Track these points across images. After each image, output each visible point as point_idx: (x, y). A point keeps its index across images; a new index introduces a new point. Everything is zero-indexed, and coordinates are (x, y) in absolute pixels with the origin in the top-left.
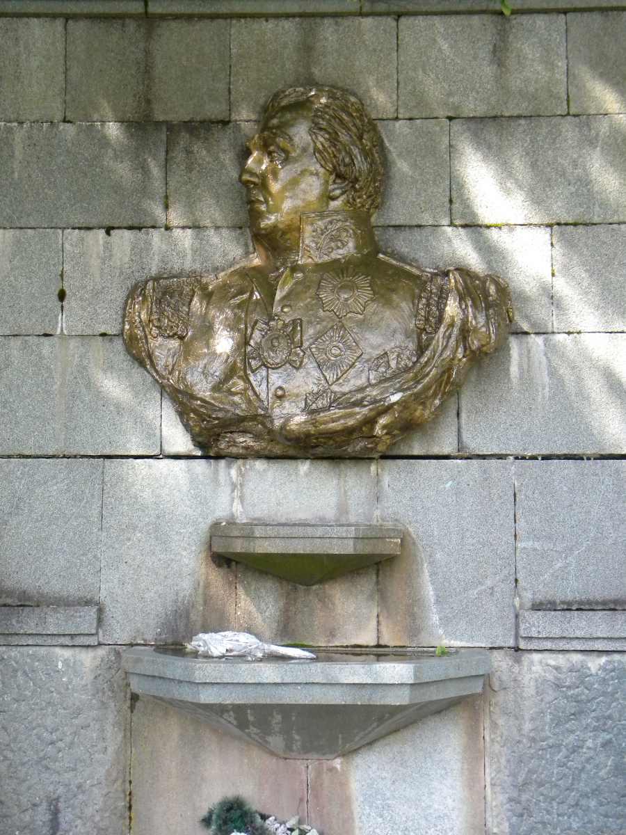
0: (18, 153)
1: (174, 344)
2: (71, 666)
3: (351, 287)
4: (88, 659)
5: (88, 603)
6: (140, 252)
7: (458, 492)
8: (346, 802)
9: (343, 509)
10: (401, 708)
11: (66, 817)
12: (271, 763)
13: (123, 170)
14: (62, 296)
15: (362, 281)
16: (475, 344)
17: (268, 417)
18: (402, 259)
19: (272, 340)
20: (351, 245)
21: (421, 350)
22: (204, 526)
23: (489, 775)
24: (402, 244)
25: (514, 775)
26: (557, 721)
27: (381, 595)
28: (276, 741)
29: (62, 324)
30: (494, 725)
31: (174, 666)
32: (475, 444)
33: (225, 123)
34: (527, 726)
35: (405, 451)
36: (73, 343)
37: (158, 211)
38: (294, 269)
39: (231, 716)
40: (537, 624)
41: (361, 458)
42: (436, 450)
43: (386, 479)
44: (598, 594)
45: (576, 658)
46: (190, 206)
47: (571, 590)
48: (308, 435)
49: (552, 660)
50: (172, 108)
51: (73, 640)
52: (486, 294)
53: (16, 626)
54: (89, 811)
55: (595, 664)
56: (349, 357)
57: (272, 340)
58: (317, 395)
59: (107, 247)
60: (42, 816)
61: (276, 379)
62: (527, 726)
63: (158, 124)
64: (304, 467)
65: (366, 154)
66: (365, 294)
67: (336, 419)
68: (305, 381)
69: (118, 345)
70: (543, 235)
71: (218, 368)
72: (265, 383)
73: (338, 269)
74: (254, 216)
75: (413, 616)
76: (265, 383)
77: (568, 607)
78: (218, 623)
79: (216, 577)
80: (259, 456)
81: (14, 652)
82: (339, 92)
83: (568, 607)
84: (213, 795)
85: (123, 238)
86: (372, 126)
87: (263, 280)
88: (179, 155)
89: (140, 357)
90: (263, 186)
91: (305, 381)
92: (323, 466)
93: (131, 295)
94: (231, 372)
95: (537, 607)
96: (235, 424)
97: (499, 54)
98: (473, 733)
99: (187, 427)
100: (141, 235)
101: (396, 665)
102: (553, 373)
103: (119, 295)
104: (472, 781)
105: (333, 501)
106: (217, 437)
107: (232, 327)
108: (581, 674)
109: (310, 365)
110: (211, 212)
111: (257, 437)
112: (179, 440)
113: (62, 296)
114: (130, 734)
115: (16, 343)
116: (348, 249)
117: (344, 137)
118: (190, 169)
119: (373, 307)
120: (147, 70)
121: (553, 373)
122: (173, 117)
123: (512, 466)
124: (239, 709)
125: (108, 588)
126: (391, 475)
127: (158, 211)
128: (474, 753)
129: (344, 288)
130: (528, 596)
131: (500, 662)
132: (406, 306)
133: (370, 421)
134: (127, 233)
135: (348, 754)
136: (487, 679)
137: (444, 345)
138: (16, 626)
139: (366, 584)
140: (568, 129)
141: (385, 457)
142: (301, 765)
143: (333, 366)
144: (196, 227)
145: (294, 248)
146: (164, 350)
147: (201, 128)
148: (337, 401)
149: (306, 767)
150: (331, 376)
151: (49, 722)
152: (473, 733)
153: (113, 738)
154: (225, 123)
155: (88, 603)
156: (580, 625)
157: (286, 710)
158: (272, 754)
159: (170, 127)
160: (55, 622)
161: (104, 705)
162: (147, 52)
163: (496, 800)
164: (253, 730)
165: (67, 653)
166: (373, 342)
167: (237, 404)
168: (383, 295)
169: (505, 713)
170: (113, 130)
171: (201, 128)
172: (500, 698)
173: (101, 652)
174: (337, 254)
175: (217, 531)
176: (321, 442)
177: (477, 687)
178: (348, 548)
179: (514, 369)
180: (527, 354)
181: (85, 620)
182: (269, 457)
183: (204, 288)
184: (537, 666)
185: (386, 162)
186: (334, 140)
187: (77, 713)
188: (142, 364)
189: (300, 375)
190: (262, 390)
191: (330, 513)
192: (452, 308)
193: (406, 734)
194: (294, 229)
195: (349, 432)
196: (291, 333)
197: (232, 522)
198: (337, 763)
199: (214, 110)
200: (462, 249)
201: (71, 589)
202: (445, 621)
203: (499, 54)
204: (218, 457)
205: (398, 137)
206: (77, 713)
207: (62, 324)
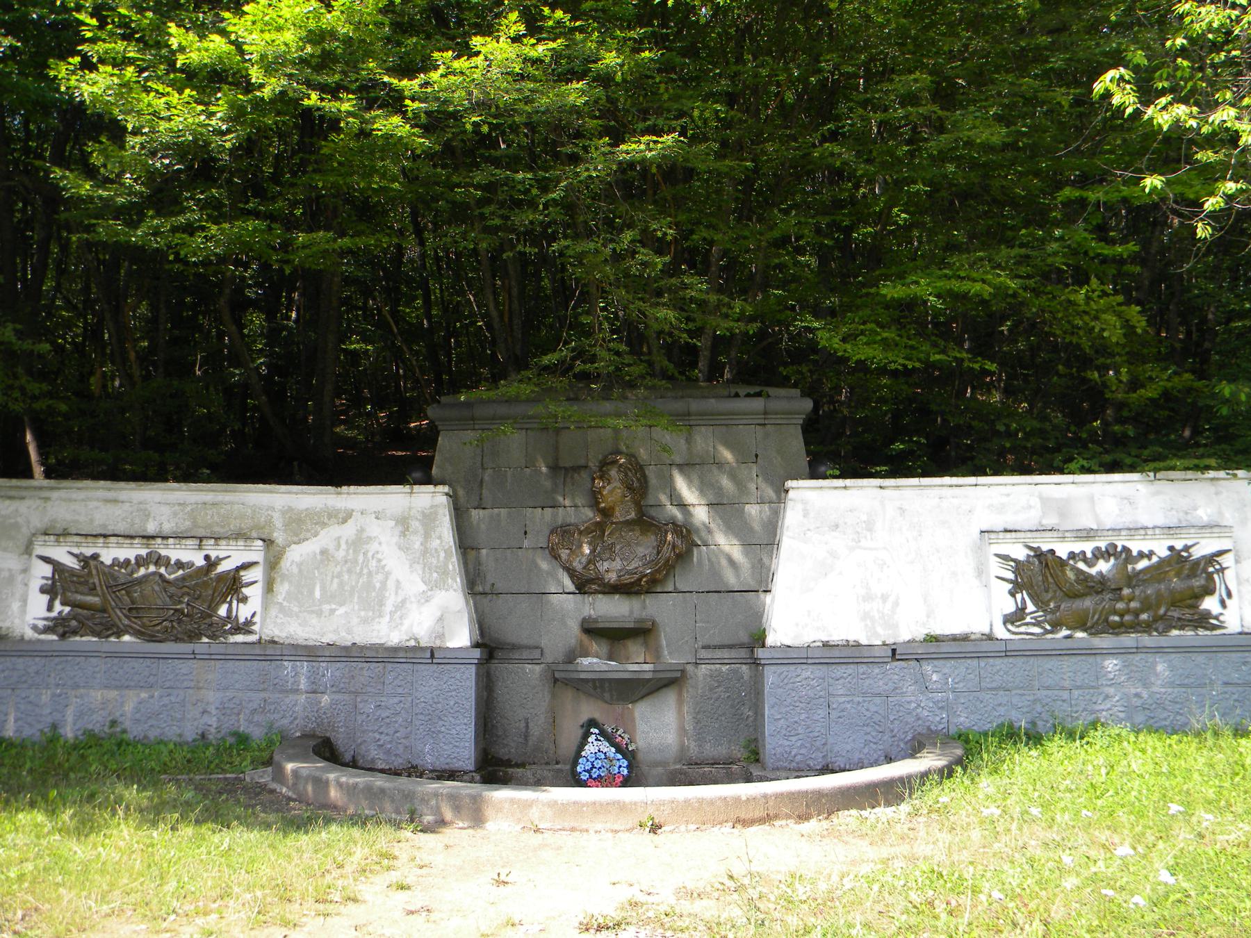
0: (509, 480)
1: (568, 551)
2: (532, 671)
3: (633, 530)
4: (537, 668)
5: (537, 648)
6: (554, 516)
7: (674, 605)
8: (633, 720)
9: (631, 612)
10: (648, 680)
11: (531, 725)
12: (606, 706)
13: (548, 484)
14: (526, 533)
15: (637, 528)
16: (677, 551)
17: (603, 579)
18: (653, 518)
19: (604, 549)
20: (633, 514)
21: (658, 553)
22: (580, 619)
23: (686, 709)
24: (653, 512)
25: (695, 709)
26: (711, 690)
27: (646, 644)
28: (607, 695)
29: (526, 544)
30: (688, 691)
31: (571, 667)
32: (681, 587)
33: (586, 467)
34: (700, 691)
35: (654, 590)
36: (530, 551)
37: (560, 499)
38: (612, 523)
39: (590, 684)
40: (704, 654)
41: (638, 593)
42: (666, 590)
43: (647, 602)
44: (726, 642)
45: (718, 666)
46: (573, 499)
47: (717, 641)
48: (617, 585)
49: (709, 667)
50: (566, 462)
51: (533, 662)
52: (682, 532)
53: (511, 656)
54: (540, 722)
55: (725, 668)
56: (632, 556)
57: (604, 549)
58: (621, 570)
59: (542, 515)
60: (523, 725)
61: (606, 565)
62: (700, 691)
63: (561, 468)
64: (617, 597)
65: (638, 480)
66: (637, 533)
67: (627, 579)
68: (617, 564)
69: (547, 551)
70: (706, 508)
71: (584, 560)
72: (603, 566)
73: (628, 523)
74: (598, 503)
75: (658, 652)
76: (603, 566)
77: (715, 647)
78: (586, 655)
79: (585, 638)
80: (600, 593)
81: (511, 666)
82: (632, 456)
83: (715, 647)
84: (584, 718)
85: (548, 511)
86: (641, 467)
87: (600, 526)
88: (568, 480)
89: (556, 557)
90: (600, 493)
91: (617, 564)
92: (624, 596)
93: (552, 532)
94: (589, 562)
95: (704, 647)
96: (591, 581)
97: (689, 441)
98: (680, 694)
99: (573, 582)
100: (555, 510)
101: (448, 517)
102: (709, 560)
103: (547, 532)
104: (680, 711)
105: (628, 609)
106: (584, 586)
107: (590, 543)
108: (720, 671)
109: (618, 559)
110: (580, 501)
111: (599, 586)
112: (570, 586)
113: (526, 533)
114: (554, 696)
115: (509, 551)
116: (633, 515)
117: (630, 474)
118: (573, 484)
119: (640, 538)
120: (556, 448)
121: (709, 560)
122: (567, 465)
123: (695, 596)
124: (594, 680)
125: (544, 642)
126: (649, 600)
127: (560, 499)
128: (680, 701)
129: (630, 531)
130: (700, 643)
131: (690, 668)
132: (653, 537)
133: (640, 580)
134: (550, 509)
135: (634, 702)
136: (683, 671)
137: (667, 552)
138: (511, 656)
139: (640, 640)
140: (714, 468)
141: (647, 592)
142: (616, 707)
143: (626, 560)
144: (576, 506)
145: (612, 515)
146: (564, 554)
147: (577, 469)
148: (630, 573)
149: (618, 708)
150: (625, 563)
151: (524, 691)
152: (680, 694)
153: (547, 697)
154: (586, 467)
155: (537, 648)
156: (719, 654)
157: (610, 681)
158: (606, 702)
159: (566, 469)
160: (526, 654)
161: (544, 685)
162: (557, 442)
163: (688, 718)
164: (598, 690)
165: (530, 666)
166: (641, 551)
167: (592, 574)
168: (644, 532)
169: (692, 687)
170: (544, 469)
171: (577, 469)
172: (690, 681)
173: (542, 666)
174: (628, 518)
175: (584, 621)
176: (1121, 221)
177: (678, 675)
178: (632, 625)
179: (695, 559)
180: (700, 553)
181: (537, 654)
182: (604, 593)
183: (579, 530)
184: (703, 669)
185: (646, 482)
186: (626, 475)
187: (534, 687)
188: (556, 559)
189: (614, 563)
190: (600, 569)
191: (627, 614)
192: (669, 537)
193: (655, 695)
194: (612, 508)
195: (632, 584)
196: (611, 548)
197: (590, 617)
198: (630, 706)
199: (582, 462)
200: (677, 513)
201: (531, 642)
202: (670, 653)
203: (689, 441)
204: (585, 593)
205: (651, 472)
206: (534, 687)
207: (526, 544)
